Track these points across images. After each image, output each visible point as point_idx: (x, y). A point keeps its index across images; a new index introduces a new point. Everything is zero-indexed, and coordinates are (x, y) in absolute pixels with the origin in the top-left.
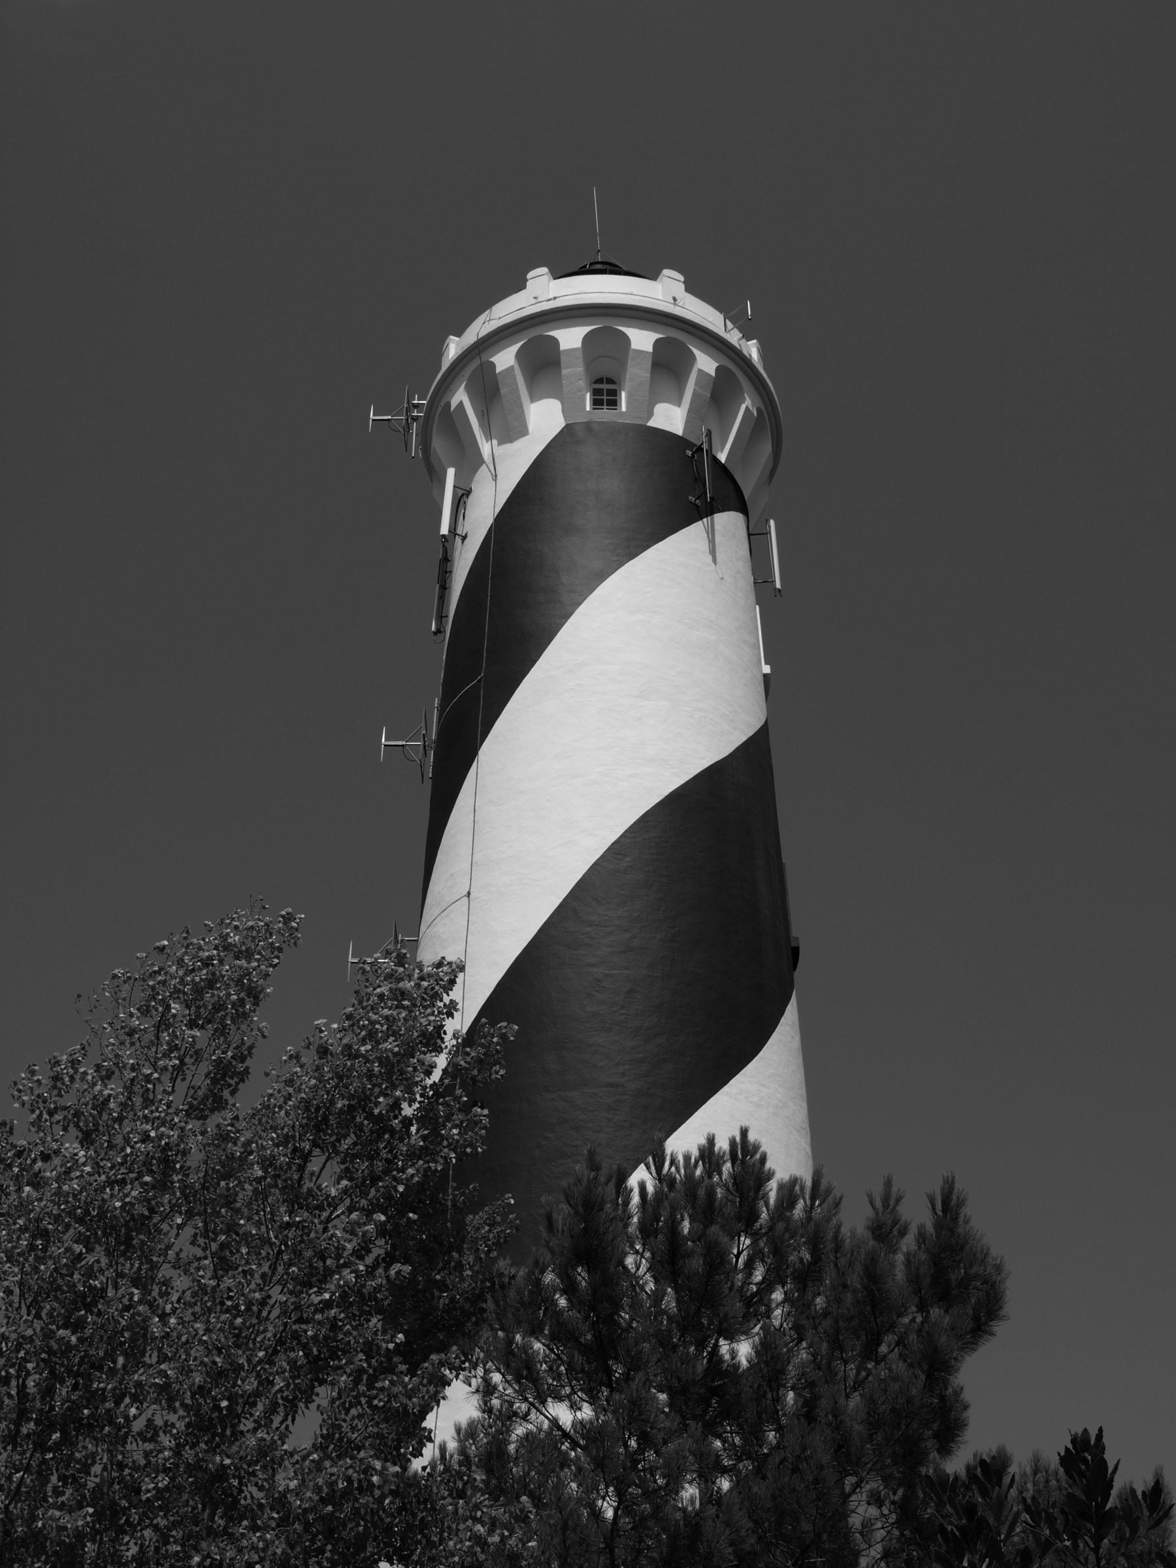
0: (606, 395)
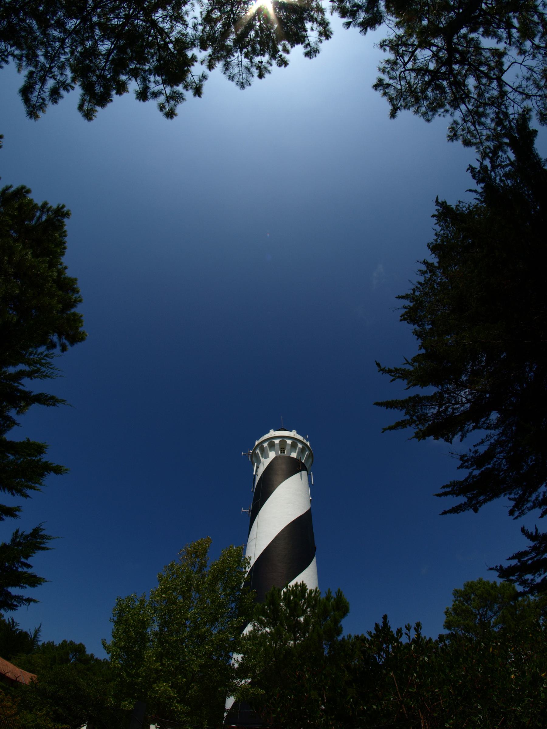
0: (283, 451)
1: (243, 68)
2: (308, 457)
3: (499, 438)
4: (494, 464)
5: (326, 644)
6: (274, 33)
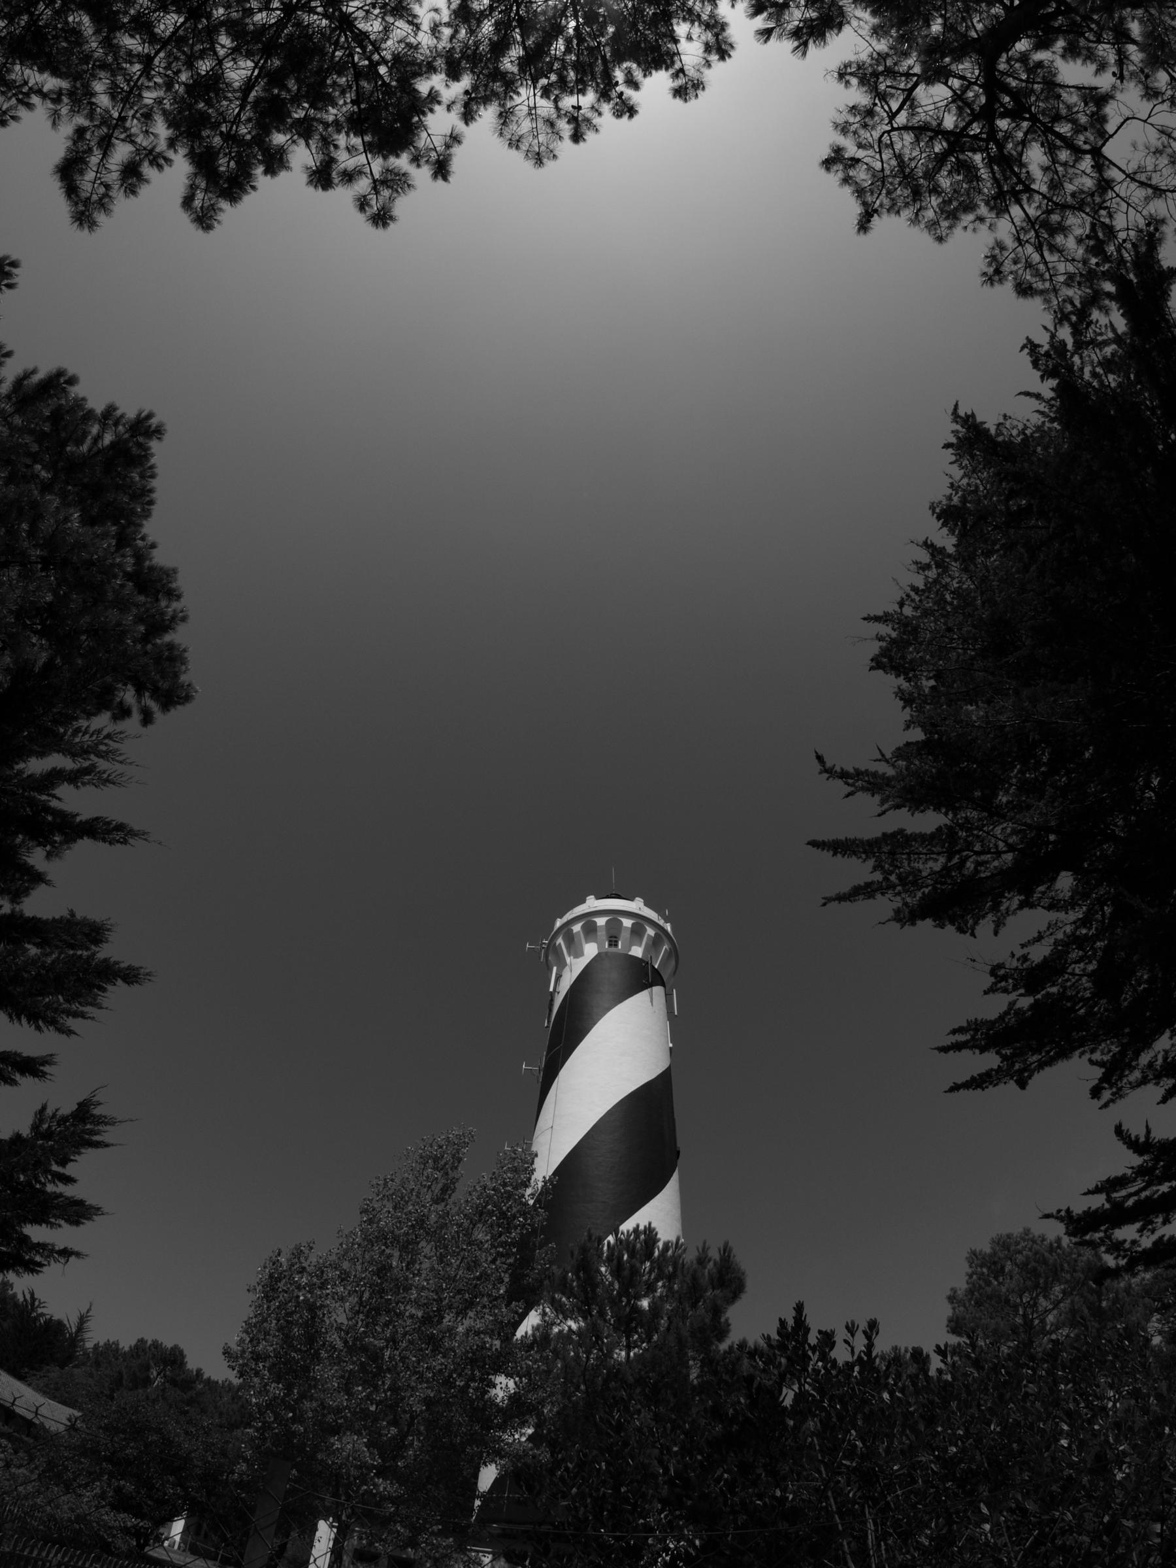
0: (613, 942)
2: (668, 955)
5: (694, 1359)
6: (607, 44)
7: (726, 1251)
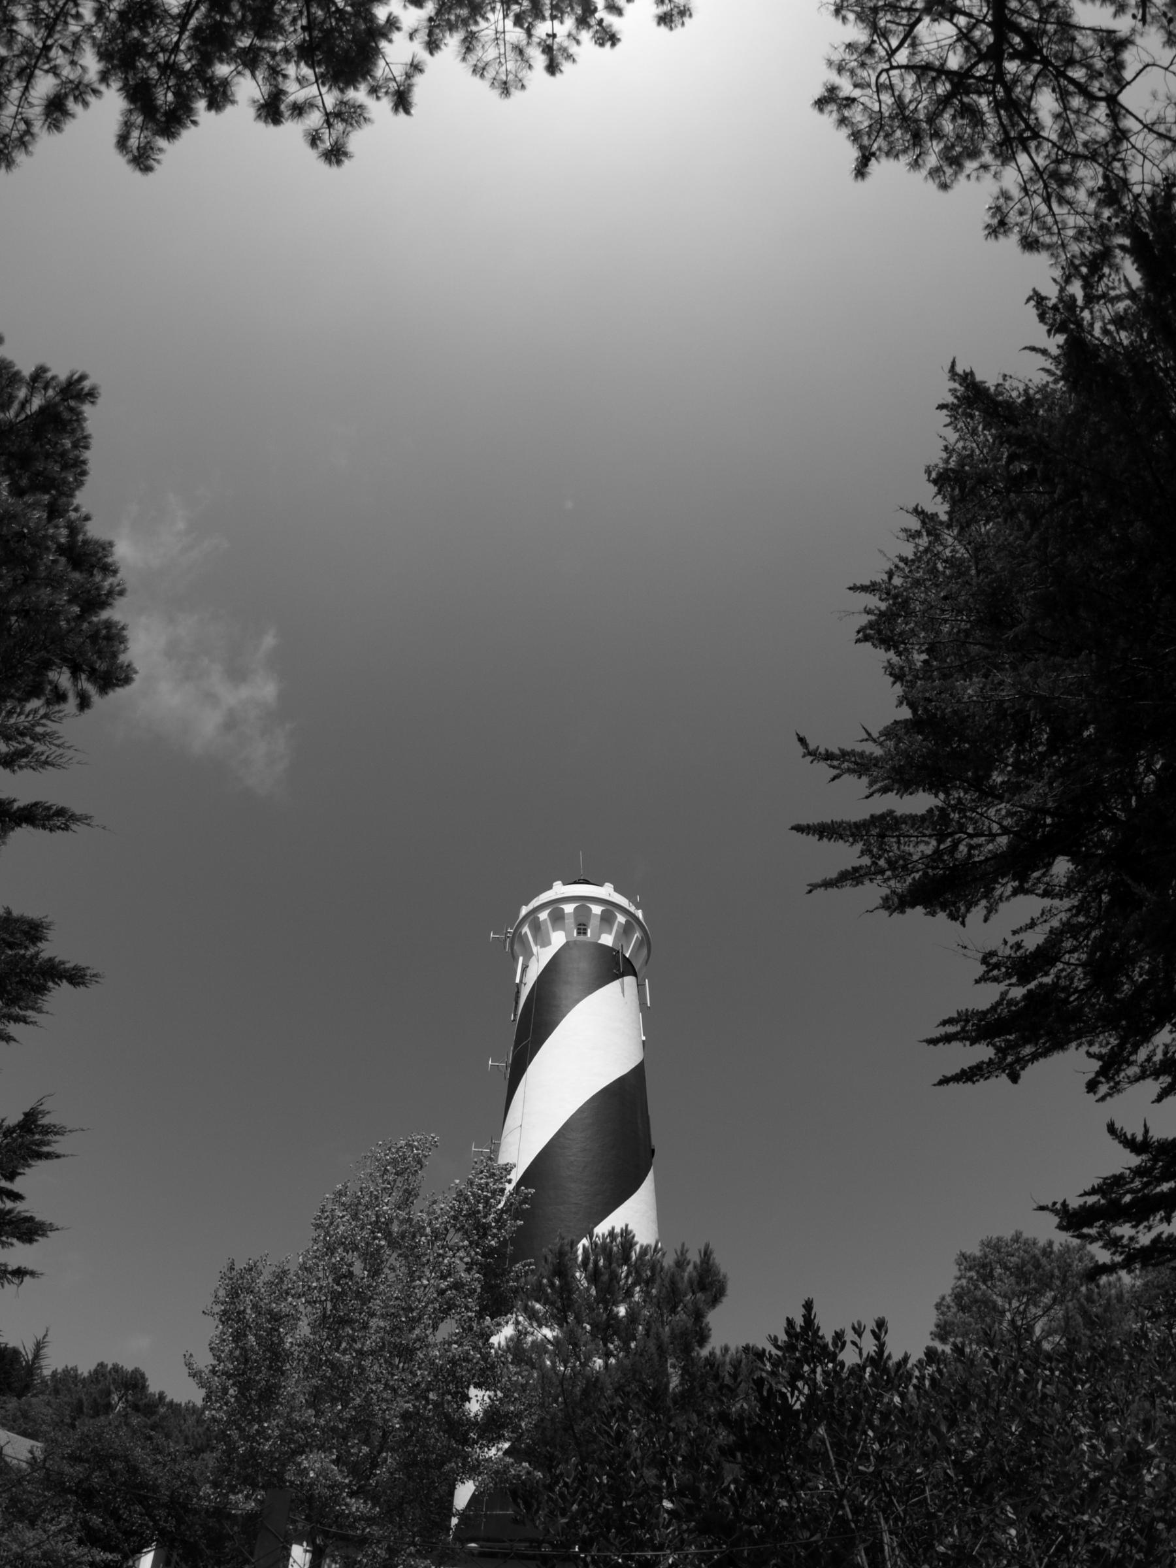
0: (582, 930)
1: (509, 47)
3: (1071, 917)
4: (1058, 977)
5: (674, 1366)
7: (707, 1254)
